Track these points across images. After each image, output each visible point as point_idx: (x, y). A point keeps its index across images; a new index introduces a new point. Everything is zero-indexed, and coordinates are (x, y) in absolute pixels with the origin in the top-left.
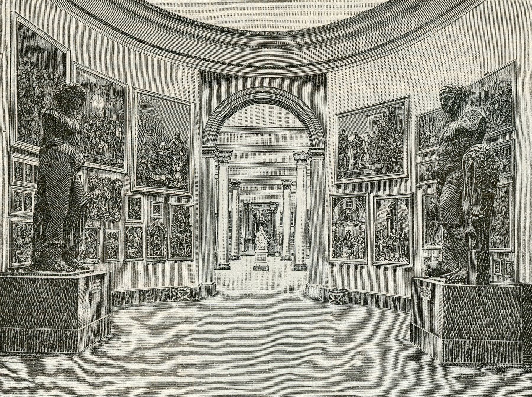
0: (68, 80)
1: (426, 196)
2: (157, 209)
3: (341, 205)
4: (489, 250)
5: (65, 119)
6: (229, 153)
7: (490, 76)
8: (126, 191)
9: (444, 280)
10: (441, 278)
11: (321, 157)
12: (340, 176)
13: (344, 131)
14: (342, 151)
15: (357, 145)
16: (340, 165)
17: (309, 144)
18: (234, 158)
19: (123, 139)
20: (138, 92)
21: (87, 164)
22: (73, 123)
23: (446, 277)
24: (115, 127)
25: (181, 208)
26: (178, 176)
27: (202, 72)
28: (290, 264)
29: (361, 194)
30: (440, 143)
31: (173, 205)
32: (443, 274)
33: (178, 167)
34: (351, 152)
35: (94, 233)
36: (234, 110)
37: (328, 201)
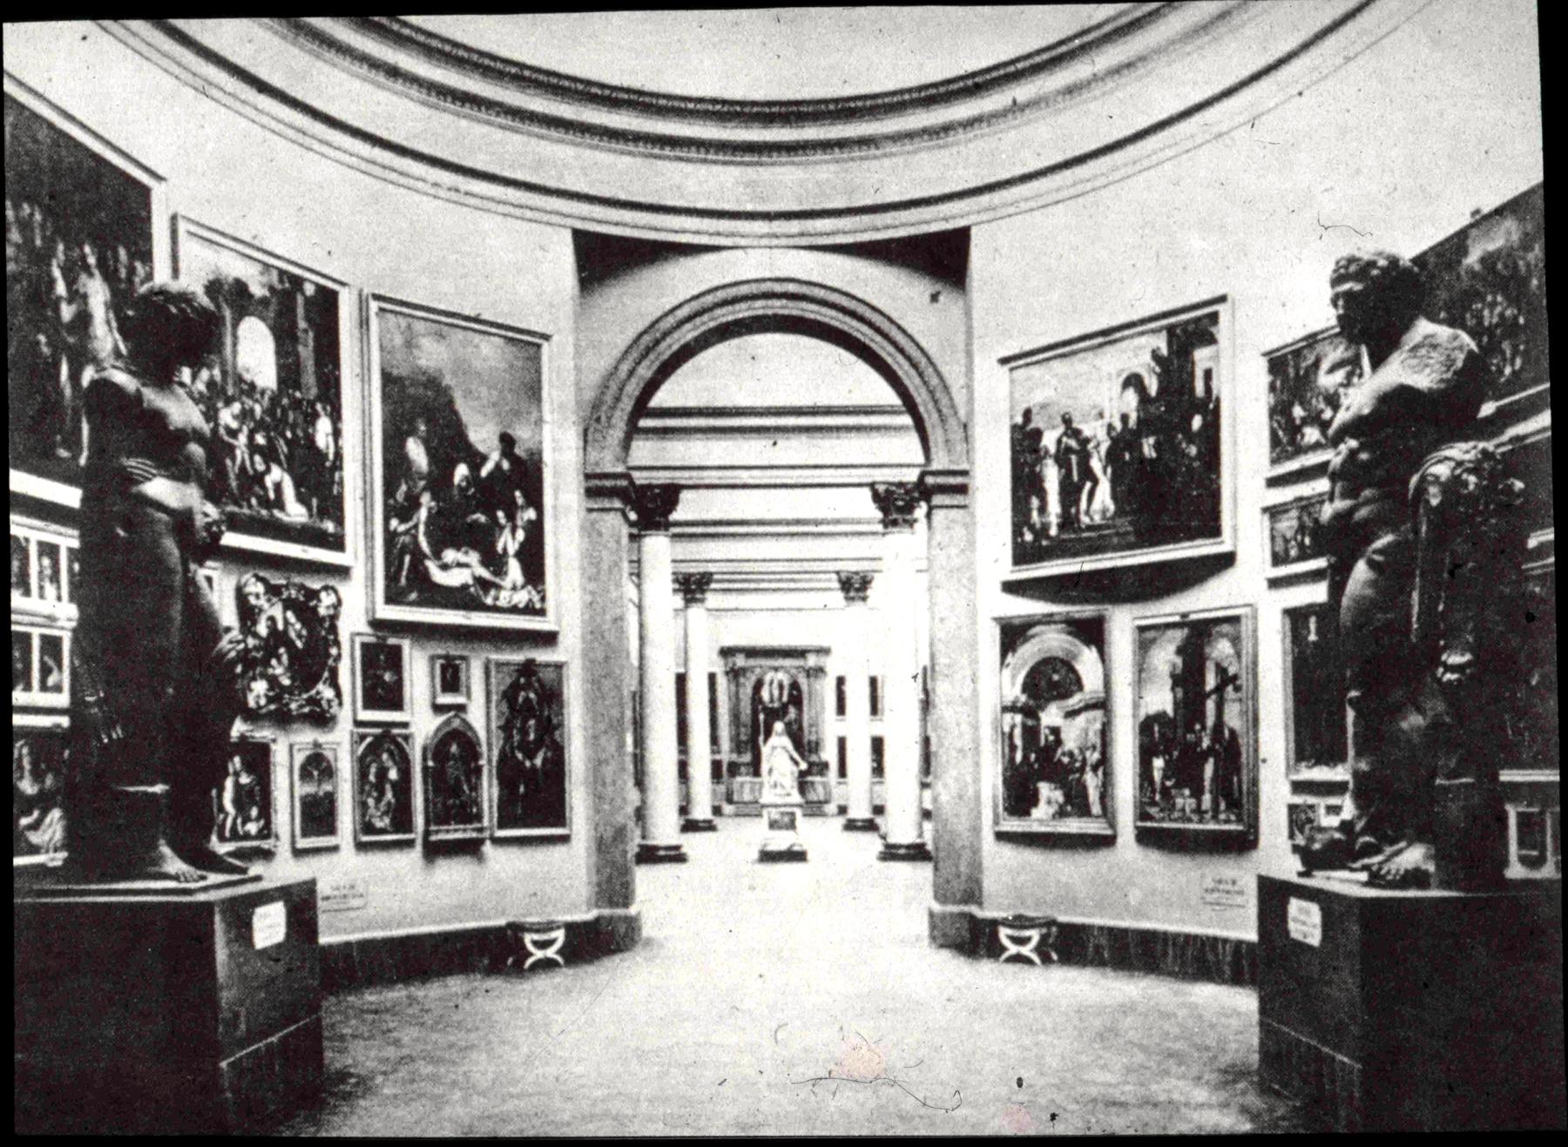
0: (162, 275)
1: (1296, 617)
2: (451, 678)
3: (1029, 653)
4: (70, 496)
5: (153, 398)
6: (670, 495)
7: (1483, 221)
8: (353, 625)
9: (1364, 876)
10: (1353, 870)
11: (958, 499)
12: (1022, 555)
13: (1027, 414)
14: (1026, 484)
15: (1074, 454)
16: (1020, 518)
17: (921, 459)
18: (688, 508)
19: (338, 455)
20: (382, 310)
21: (231, 539)
22: (182, 411)
23: (1365, 868)
24: (312, 418)
25: (528, 668)
26: (514, 571)
27: (578, 234)
28: (871, 844)
29: (1086, 611)
30: (1335, 441)
31: (499, 665)
32: (1357, 857)
33: (509, 542)
34: (1052, 476)
35: (258, 759)
36: (686, 353)
37: (990, 639)
